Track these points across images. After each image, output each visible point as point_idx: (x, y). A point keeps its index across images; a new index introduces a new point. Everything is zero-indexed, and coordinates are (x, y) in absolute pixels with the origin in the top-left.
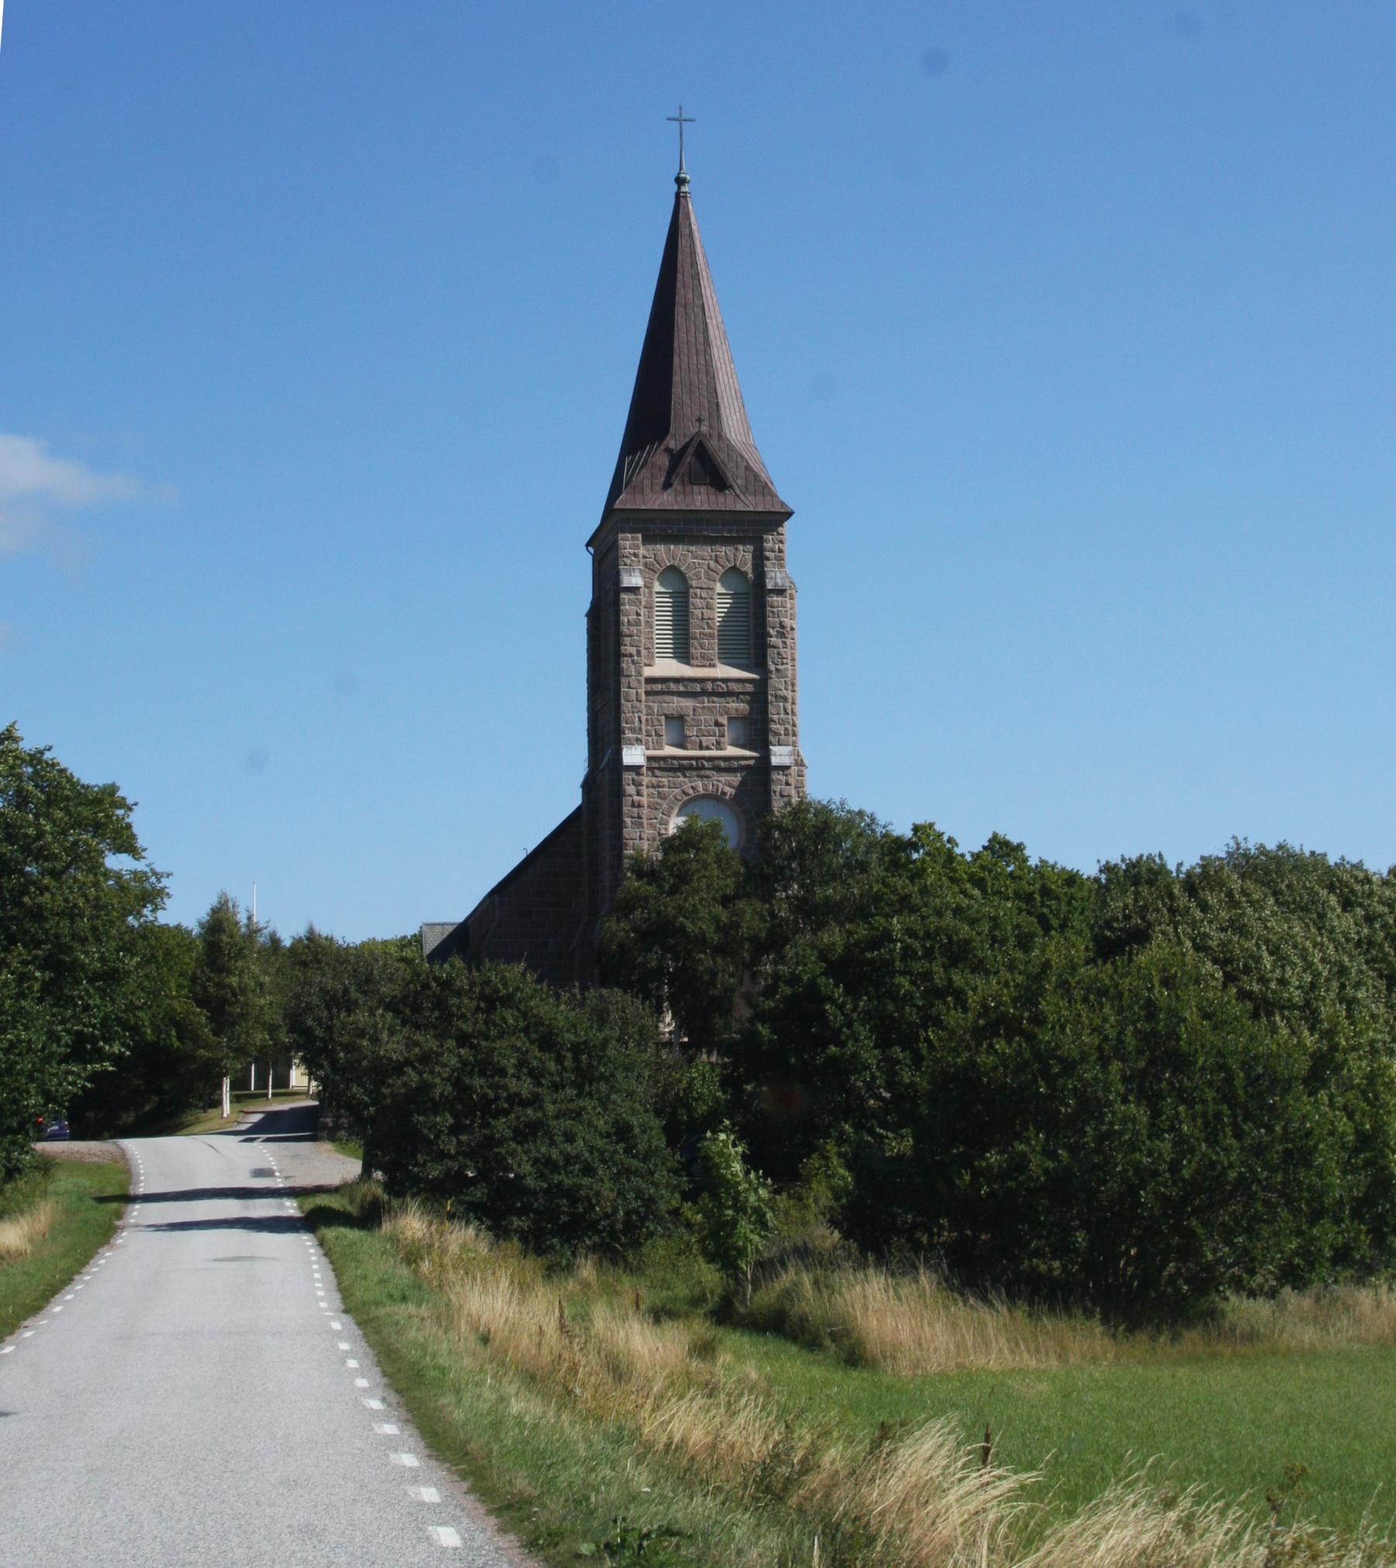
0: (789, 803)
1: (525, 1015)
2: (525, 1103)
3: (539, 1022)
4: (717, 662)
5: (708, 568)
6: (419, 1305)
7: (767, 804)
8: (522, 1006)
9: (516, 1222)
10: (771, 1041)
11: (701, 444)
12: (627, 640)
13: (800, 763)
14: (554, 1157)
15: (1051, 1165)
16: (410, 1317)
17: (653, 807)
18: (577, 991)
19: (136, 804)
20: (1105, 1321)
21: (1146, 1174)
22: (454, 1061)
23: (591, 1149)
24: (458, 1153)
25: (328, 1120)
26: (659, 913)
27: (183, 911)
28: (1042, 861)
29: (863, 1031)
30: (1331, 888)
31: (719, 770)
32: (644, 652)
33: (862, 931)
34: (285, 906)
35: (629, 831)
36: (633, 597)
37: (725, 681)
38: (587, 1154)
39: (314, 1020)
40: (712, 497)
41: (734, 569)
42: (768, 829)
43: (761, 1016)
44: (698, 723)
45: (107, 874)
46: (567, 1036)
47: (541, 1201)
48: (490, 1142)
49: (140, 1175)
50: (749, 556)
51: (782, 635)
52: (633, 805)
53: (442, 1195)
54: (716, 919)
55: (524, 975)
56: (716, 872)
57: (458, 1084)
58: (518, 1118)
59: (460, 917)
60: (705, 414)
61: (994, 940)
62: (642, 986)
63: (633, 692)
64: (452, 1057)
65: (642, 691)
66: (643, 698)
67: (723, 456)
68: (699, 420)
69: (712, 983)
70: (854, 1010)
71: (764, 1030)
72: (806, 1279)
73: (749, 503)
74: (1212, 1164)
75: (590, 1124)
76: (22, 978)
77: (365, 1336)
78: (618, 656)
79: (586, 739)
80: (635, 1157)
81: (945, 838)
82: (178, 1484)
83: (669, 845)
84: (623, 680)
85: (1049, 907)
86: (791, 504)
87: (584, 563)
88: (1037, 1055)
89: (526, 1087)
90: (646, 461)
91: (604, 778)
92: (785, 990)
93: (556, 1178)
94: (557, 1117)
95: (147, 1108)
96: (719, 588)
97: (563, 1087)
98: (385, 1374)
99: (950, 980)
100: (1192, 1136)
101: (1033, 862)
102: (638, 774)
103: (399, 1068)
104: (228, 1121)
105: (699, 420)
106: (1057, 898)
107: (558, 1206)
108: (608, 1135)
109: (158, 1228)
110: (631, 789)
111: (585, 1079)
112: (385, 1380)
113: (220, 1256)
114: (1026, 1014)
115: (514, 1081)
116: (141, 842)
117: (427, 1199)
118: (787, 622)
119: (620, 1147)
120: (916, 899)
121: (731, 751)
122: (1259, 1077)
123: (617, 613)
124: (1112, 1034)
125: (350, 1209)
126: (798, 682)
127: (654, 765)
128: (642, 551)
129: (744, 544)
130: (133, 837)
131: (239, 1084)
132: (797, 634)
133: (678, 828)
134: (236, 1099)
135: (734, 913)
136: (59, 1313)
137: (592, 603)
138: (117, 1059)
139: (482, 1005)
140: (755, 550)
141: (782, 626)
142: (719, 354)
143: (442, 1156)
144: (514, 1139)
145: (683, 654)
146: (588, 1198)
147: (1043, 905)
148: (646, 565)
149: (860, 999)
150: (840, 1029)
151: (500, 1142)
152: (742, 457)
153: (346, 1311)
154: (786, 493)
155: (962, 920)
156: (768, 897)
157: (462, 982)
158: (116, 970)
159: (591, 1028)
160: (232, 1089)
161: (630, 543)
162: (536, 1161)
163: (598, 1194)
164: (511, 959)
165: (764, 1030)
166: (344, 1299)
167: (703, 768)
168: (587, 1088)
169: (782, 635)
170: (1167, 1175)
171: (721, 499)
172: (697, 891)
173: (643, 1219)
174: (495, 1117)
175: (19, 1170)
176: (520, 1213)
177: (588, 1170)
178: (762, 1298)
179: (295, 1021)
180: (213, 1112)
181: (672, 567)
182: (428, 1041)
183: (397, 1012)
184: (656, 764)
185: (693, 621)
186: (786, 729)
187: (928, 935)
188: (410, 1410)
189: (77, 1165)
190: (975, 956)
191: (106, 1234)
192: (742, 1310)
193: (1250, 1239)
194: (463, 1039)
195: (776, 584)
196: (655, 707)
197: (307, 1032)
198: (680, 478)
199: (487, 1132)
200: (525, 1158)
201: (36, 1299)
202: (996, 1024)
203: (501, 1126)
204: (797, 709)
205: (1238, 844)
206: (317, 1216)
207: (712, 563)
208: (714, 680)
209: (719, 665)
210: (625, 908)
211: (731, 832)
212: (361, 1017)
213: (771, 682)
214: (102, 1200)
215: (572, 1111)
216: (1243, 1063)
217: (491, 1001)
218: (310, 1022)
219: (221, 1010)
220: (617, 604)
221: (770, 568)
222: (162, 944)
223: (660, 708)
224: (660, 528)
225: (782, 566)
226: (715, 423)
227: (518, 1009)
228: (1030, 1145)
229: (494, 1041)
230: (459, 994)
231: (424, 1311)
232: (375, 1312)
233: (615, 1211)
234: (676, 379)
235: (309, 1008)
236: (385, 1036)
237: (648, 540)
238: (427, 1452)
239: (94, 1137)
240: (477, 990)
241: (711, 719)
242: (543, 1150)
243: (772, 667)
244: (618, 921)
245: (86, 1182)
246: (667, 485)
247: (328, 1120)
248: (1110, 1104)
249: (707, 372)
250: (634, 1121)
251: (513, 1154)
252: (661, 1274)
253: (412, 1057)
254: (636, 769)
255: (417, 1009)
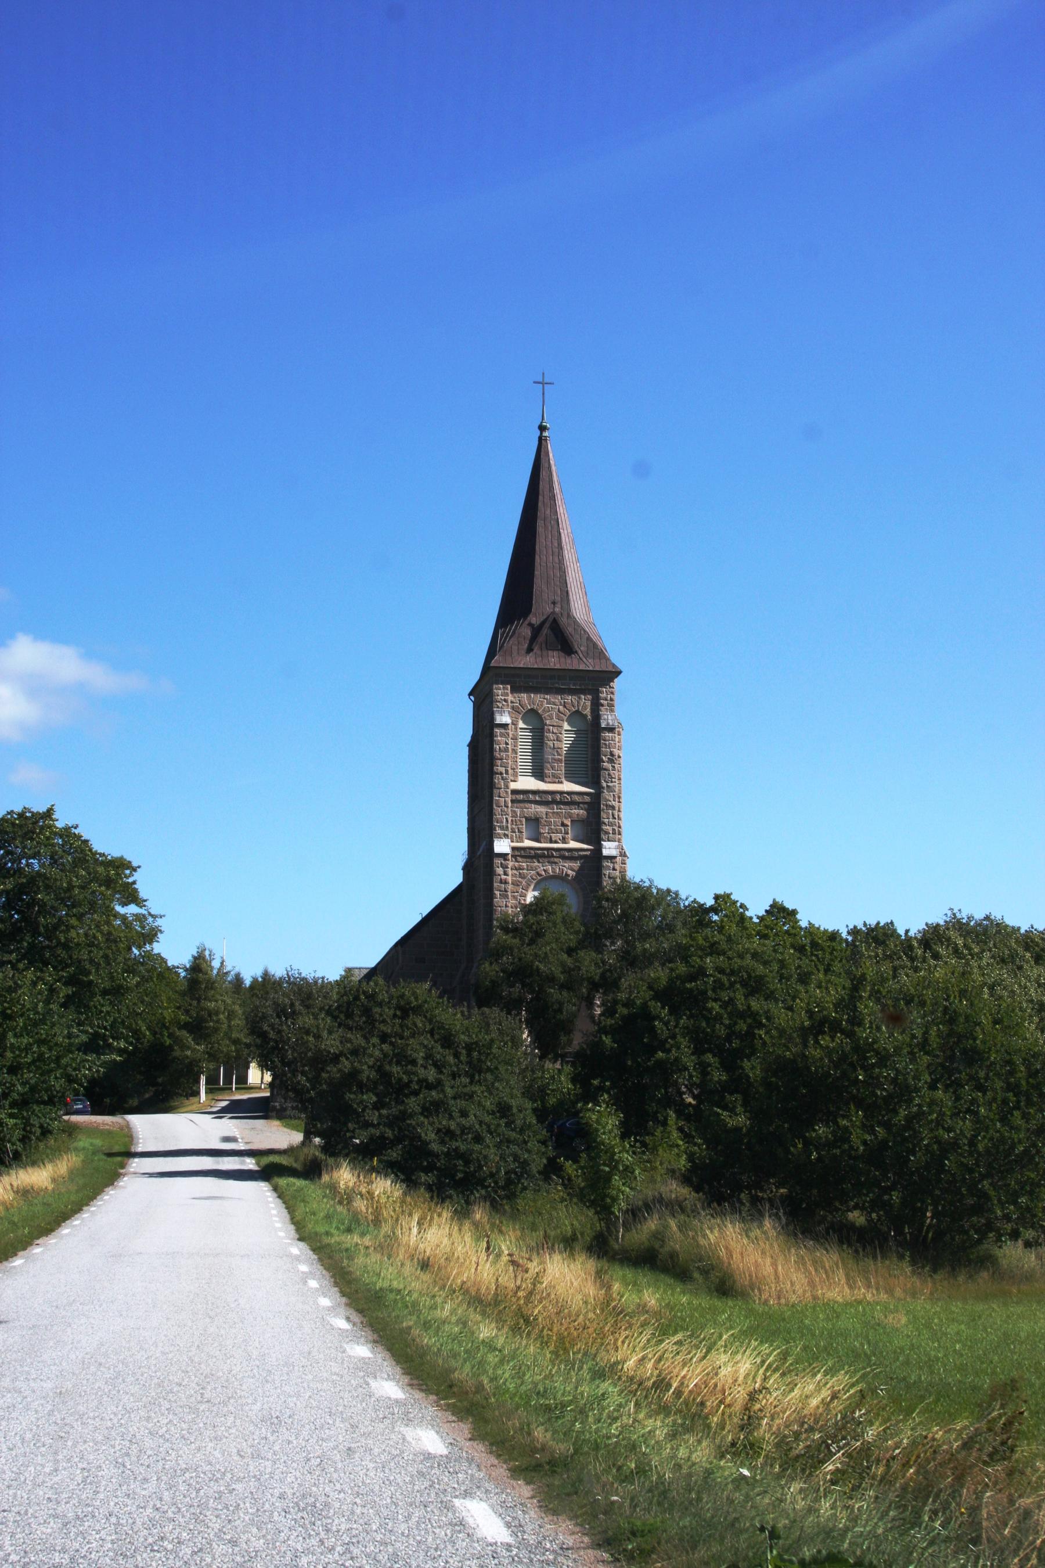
0: (615, 882)
1: (430, 1021)
2: (430, 1087)
3: (441, 1027)
4: (563, 780)
6: (363, 1235)
7: (598, 882)
8: (428, 1015)
9: (423, 1177)
10: (612, 1048)
11: (555, 621)
12: (499, 762)
13: (623, 855)
14: (452, 1128)
15: (868, 1137)
16: (357, 1244)
17: (515, 884)
18: (465, 1009)
19: (139, 867)
20: (913, 1262)
21: (949, 1148)
22: (377, 1053)
23: (481, 1123)
24: (379, 1124)
25: (277, 1104)
26: (520, 959)
27: (175, 950)
28: (810, 923)
29: (684, 1042)
30: (1027, 948)
31: (564, 858)
32: (510, 771)
33: (682, 969)
34: (249, 955)
35: (498, 900)
37: (570, 793)
38: (477, 1126)
39: (269, 1026)
40: (563, 660)
41: (577, 712)
42: (599, 900)
43: (603, 1030)
44: (549, 824)
45: (117, 915)
46: (462, 1037)
47: (443, 1162)
48: (404, 1116)
49: (138, 1143)
50: (589, 703)
51: (611, 761)
52: (501, 882)
53: (368, 1155)
54: (563, 964)
55: (430, 991)
56: (563, 929)
57: (380, 1070)
58: (425, 1098)
59: (373, 965)
60: (558, 599)
61: (782, 977)
62: (511, 1006)
63: (502, 800)
64: (376, 1050)
65: (509, 800)
66: (510, 805)
67: (570, 629)
68: (554, 603)
69: (560, 1010)
70: (676, 1027)
71: (607, 1040)
72: (673, 1224)
73: (589, 665)
74: (1002, 1140)
75: (480, 1104)
76: (52, 990)
77: (320, 1260)
78: (492, 773)
80: (512, 1130)
81: (738, 904)
82: (148, 1419)
83: (527, 910)
84: (495, 791)
85: (816, 956)
86: (620, 666)
87: (467, 708)
88: (857, 1049)
89: (431, 1074)
90: (514, 632)
91: (480, 862)
92: (622, 1011)
93: (454, 1144)
94: (454, 1098)
95: (147, 1096)
96: (566, 726)
97: (459, 1076)
98: (343, 1294)
99: (749, 1007)
100: (988, 1117)
101: (804, 924)
102: (505, 860)
103: (336, 1059)
104: (204, 1105)
105: (554, 603)
106: (822, 949)
107: (455, 1165)
108: (493, 1113)
109: (151, 1175)
110: (500, 871)
111: (475, 1070)
112: (344, 1300)
113: (198, 1196)
114: (845, 1017)
115: (423, 1070)
116: (143, 894)
117: (355, 1158)
118: (616, 752)
119: (503, 1122)
120: (724, 946)
121: (573, 844)
122: (1037, 1071)
123: (492, 742)
124: (918, 1033)
125: (295, 1165)
126: (622, 796)
127: (517, 853)
128: (510, 698)
129: (585, 694)
130: (136, 891)
131: (212, 1081)
132: (622, 761)
133: (535, 897)
134: (209, 1091)
135: (577, 960)
136: (67, 1235)
137: (472, 737)
138: (121, 1051)
139: (398, 1013)
141: (612, 754)
142: (569, 555)
143: (367, 1125)
144: (422, 1114)
145: (539, 773)
146: (478, 1160)
147: (812, 954)
148: (513, 708)
149: (681, 1018)
150: (666, 1040)
151: (411, 1116)
152: (585, 631)
153: (300, 1239)
154: (616, 656)
155: (757, 961)
156: (599, 949)
157: (383, 996)
158: (121, 986)
159: (480, 1031)
160: (206, 1084)
161: (502, 692)
162: (439, 1131)
163: (485, 1157)
164: (421, 978)
165: (607, 1040)
166: (298, 1230)
167: (553, 856)
168: (477, 1077)
169: (611, 761)
170: (966, 1148)
171: (569, 661)
172: (548, 944)
173: (519, 1177)
174: (407, 1096)
175: (50, 1132)
176: (427, 1170)
177: (478, 1139)
178: (626, 1238)
179: (254, 1026)
180: (193, 1100)
181: (532, 710)
182: (358, 1039)
183: (335, 1018)
184: (519, 853)
185: (547, 750)
186: (614, 830)
187: (733, 972)
188: (375, 1330)
189: (93, 1131)
190: (768, 988)
191: (112, 1178)
192: (616, 1247)
193: (1032, 1201)
194: (384, 1038)
195: (608, 724)
196: (518, 811)
197: (263, 1035)
198: (540, 650)
199: (402, 1108)
200: (430, 1128)
201: (49, 1224)
202: (820, 1026)
203: (413, 1104)
204: (622, 815)
205: (954, 914)
206: (270, 1169)
208: (561, 793)
209: (565, 782)
210: (496, 955)
211: (573, 903)
212: (307, 1021)
213: (603, 795)
214: (110, 1155)
215: (466, 1094)
216: (1024, 1060)
217: (405, 1011)
218: (266, 1028)
219: (198, 1028)
220: (491, 735)
221: (603, 711)
222: (158, 971)
223: (522, 812)
224: (524, 681)
225: (612, 711)
226: (565, 606)
227: (425, 1017)
228: (851, 1120)
229: (408, 1039)
230: (380, 1004)
231: (367, 1241)
232: (327, 1240)
233: (498, 1170)
234: (537, 573)
235: (264, 1017)
236: (325, 1034)
237: (514, 690)
238: (406, 1379)
239: (111, 1113)
240: (394, 1002)
241: (559, 821)
242: (444, 1123)
243: (604, 784)
244: (491, 964)
245: (98, 1142)
246: (530, 650)
247: (277, 1104)
248: (917, 1090)
249: (560, 568)
250: (513, 1103)
251: (421, 1125)
252: (530, 1219)
253: (346, 1051)
254: (504, 856)
255: (349, 1015)
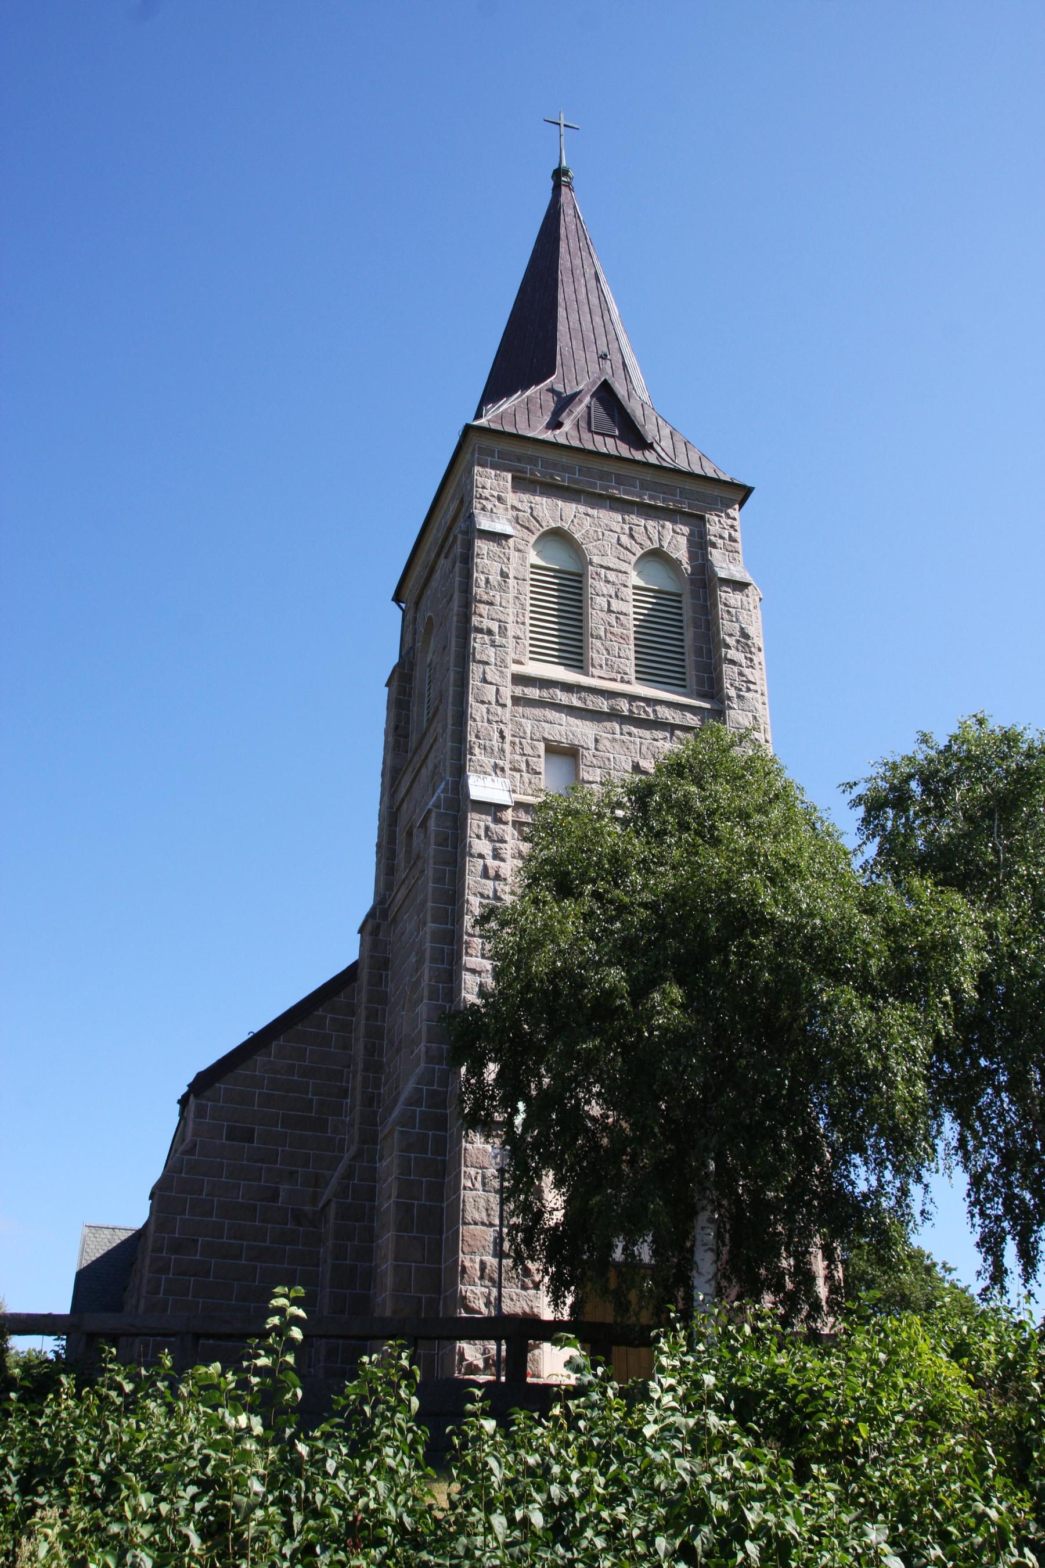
5: (618, 547)
36: (493, 547)
50: (683, 541)
52: (485, 874)
79: (373, 859)
84: (475, 671)
110: (482, 846)
128: (512, 498)
129: (674, 522)
140: (691, 534)
196: (528, 725)
207: (625, 540)
237: (521, 484)
254: (494, 809)
